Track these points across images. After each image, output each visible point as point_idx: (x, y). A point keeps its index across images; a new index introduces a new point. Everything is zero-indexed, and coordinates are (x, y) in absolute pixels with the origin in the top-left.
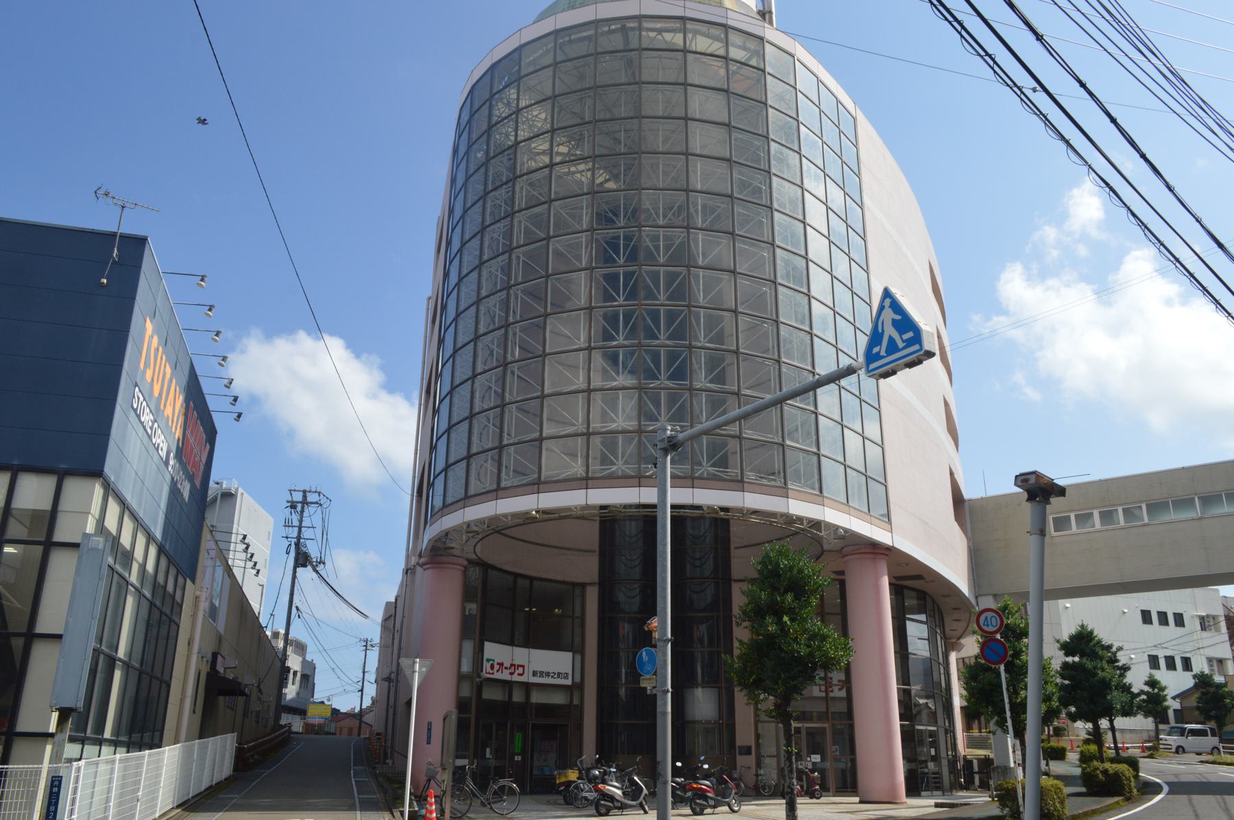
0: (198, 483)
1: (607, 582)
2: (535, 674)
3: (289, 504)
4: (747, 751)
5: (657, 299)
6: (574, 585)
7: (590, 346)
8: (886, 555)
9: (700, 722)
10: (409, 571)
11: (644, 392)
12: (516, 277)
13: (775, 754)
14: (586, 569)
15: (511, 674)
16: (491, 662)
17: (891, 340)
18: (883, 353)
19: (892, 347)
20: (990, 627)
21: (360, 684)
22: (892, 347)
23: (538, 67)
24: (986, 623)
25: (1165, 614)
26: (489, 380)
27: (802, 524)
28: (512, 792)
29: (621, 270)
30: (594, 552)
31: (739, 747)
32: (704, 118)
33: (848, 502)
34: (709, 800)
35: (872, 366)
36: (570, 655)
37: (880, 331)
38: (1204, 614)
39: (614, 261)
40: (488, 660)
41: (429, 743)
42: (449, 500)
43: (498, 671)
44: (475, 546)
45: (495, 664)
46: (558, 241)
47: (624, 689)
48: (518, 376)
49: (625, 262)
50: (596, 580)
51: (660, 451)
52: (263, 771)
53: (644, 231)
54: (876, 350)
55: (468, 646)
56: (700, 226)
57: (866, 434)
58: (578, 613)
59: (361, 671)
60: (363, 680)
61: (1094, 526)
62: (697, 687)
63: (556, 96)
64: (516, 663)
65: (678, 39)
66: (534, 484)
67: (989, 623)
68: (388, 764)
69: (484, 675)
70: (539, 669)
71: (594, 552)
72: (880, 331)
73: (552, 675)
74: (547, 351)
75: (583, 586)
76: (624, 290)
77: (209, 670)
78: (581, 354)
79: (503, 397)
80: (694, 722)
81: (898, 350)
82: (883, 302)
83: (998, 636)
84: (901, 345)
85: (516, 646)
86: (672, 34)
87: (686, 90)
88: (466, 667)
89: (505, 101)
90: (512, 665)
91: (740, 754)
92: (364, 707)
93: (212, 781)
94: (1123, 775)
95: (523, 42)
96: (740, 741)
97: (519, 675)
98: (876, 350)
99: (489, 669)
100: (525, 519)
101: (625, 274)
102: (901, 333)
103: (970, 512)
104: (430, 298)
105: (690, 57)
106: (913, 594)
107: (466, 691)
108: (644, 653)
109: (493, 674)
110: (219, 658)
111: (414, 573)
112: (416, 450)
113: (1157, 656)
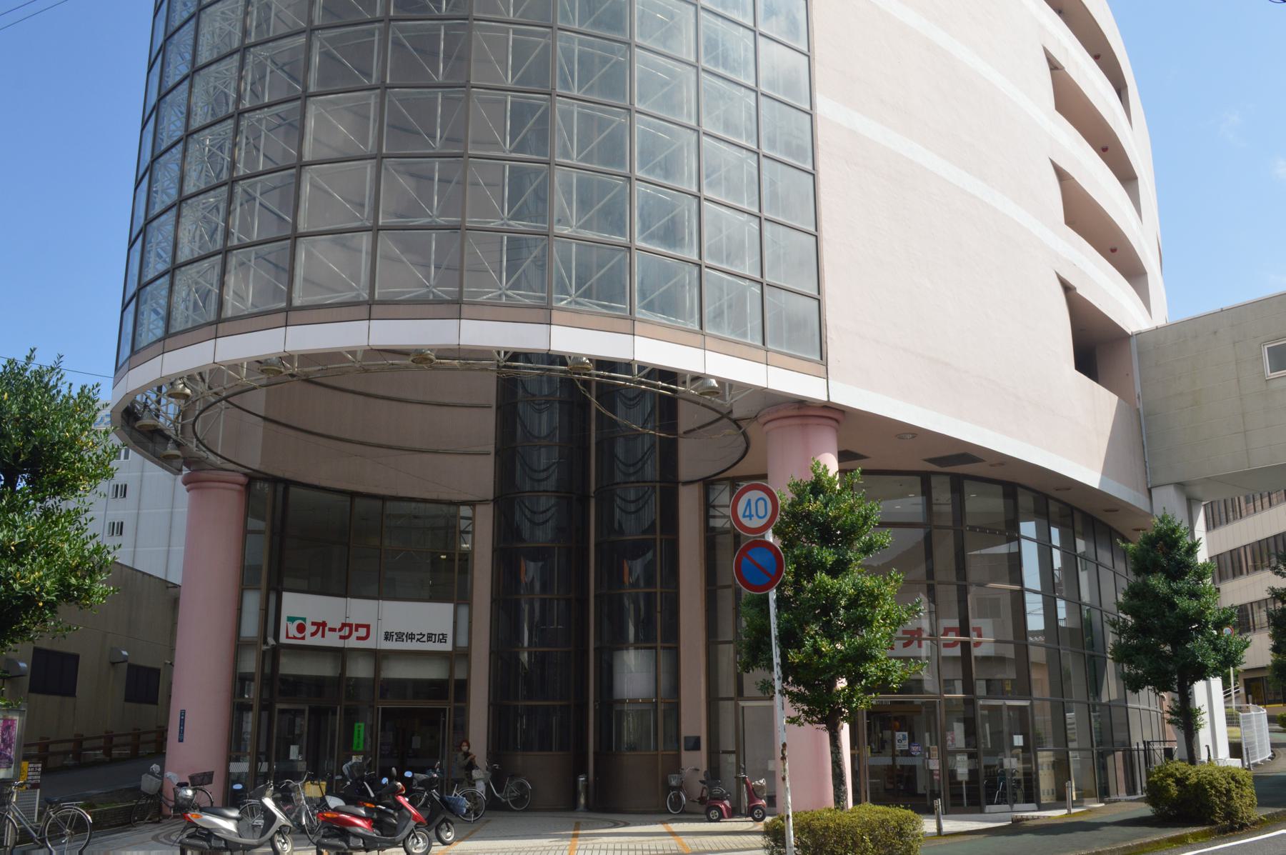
2: (388, 636)
4: (694, 744)
8: (837, 420)
9: (634, 701)
20: (755, 518)
24: (747, 513)
27: (631, 373)
28: (79, 825)
31: (685, 738)
33: (764, 344)
34: (351, 838)
40: (291, 619)
41: (181, 740)
47: (526, 655)
48: (260, 204)
55: (252, 601)
62: (627, 649)
67: (753, 512)
70: (395, 629)
73: (417, 637)
79: (227, 234)
80: (622, 701)
83: (770, 537)
88: (250, 628)
90: (344, 625)
91: (686, 750)
94: (1213, 787)
96: (687, 730)
97: (359, 638)
107: (250, 664)
109: (303, 638)
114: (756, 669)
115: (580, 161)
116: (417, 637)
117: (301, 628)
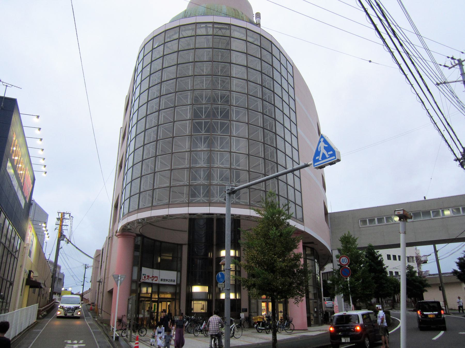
0: (28, 200)
1: (191, 244)
2: (162, 280)
3: (298, 247)
5: (217, 133)
6: (178, 244)
7: (191, 150)
10: (110, 238)
11: (212, 169)
12: (161, 122)
13: (256, 311)
14: (183, 238)
15: (152, 280)
16: (145, 275)
17: (323, 154)
18: (320, 159)
19: (324, 157)
20: (344, 262)
21: (83, 282)
22: (324, 157)
23: (171, 39)
25: (395, 256)
26: (149, 162)
29: (203, 121)
30: (186, 231)
31: (242, 309)
32: (237, 63)
35: (316, 164)
36: (175, 273)
37: (319, 151)
38: (409, 256)
39: (201, 117)
40: (143, 275)
42: (131, 210)
43: (147, 279)
44: (140, 229)
45: (146, 276)
46: (178, 108)
49: (205, 117)
50: (187, 243)
51: (227, 194)
52: (48, 319)
53: (213, 106)
54: (317, 158)
55: (136, 269)
56: (234, 105)
57: (295, 188)
58: (179, 256)
59: (83, 277)
60: (84, 281)
61: (375, 224)
63: (179, 51)
64: (154, 275)
65: (227, 33)
66: (167, 205)
68: (100, 316)
69: (142, 281)
71: (186, 231)
72: (319, 151)
73: (168, 280)
74: (173, 151)
75: (181, 245)
76: (204, 129)
77: (27, 278)
78: (186, 154)
81: (326, 158)
82: (320, 139)
83: (347, 266)
84: (327, 156)
85: (155, 269)
86: (225, 30)
87: (230, 52)
88: (135, 277)
89: (158, 52)
90: (152, 277)
92: (84, 292)
93: (29, 324)
95: (166, 29)
97: (155, 280)
98: (317, 158)
99: (144, 278)
100: (165, 218)
101: (205, 122)
102: (327, 152)
103: (330, 218)
104: (121, 128)
105: (232, 39)
106: (309, 249)
108: (220, 274)
109: (145, 280)
110: (32, 273)
111: (112, 239)
112: (114, 189)
113: (392, 272)
114: (342, 236)
115: (236, 150)
116: (168, 280)
117: (145, 277)
